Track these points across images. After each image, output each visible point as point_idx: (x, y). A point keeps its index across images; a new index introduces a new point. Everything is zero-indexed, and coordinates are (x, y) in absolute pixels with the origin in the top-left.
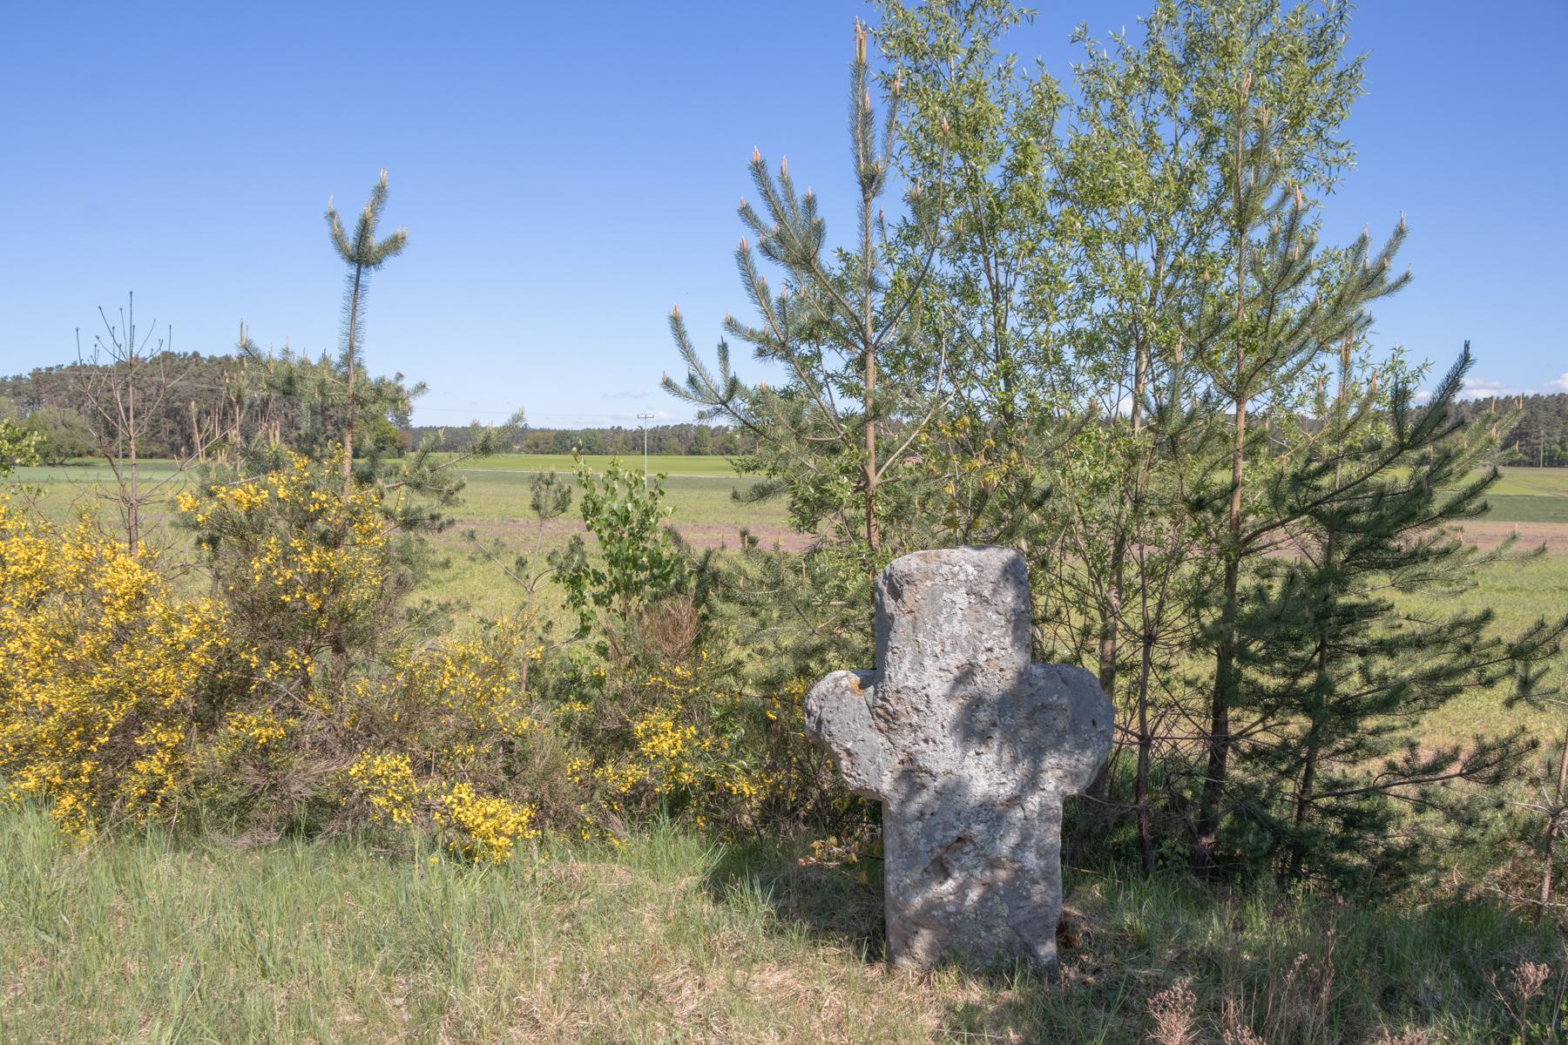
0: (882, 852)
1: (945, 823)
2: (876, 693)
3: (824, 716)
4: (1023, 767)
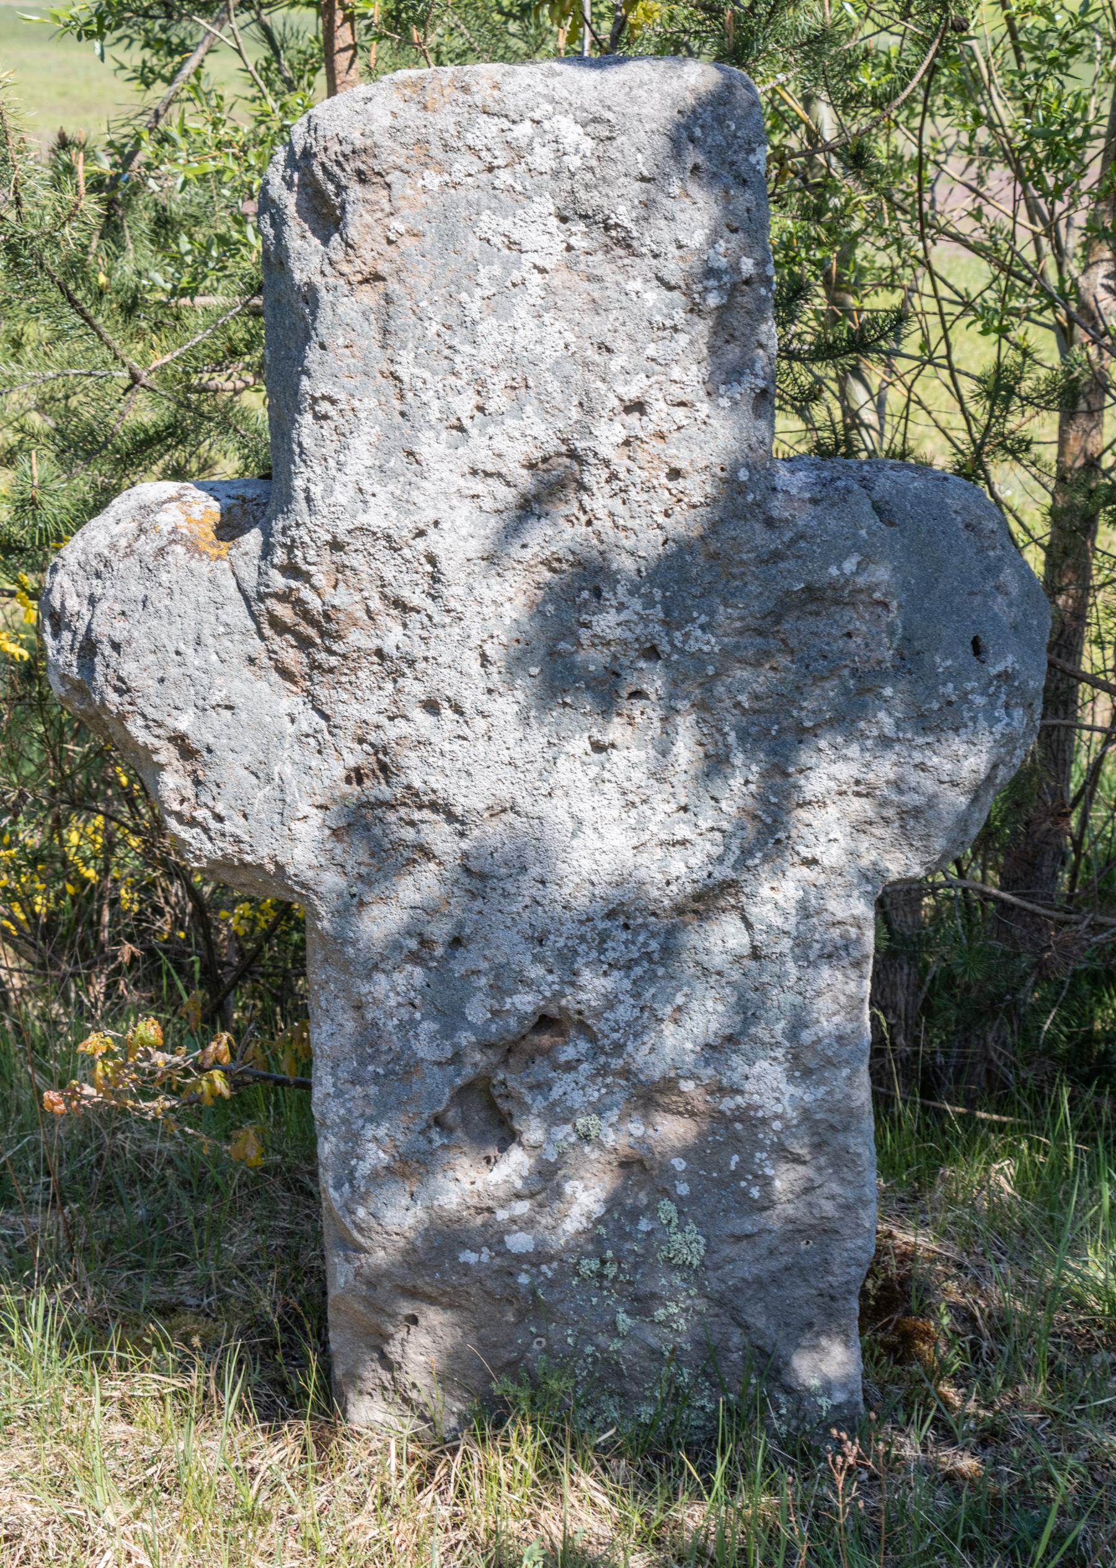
0: (306, 1064)
1: (499, 971)
2: (267, 550)
3: (102, 630)
4: (740, 786)
